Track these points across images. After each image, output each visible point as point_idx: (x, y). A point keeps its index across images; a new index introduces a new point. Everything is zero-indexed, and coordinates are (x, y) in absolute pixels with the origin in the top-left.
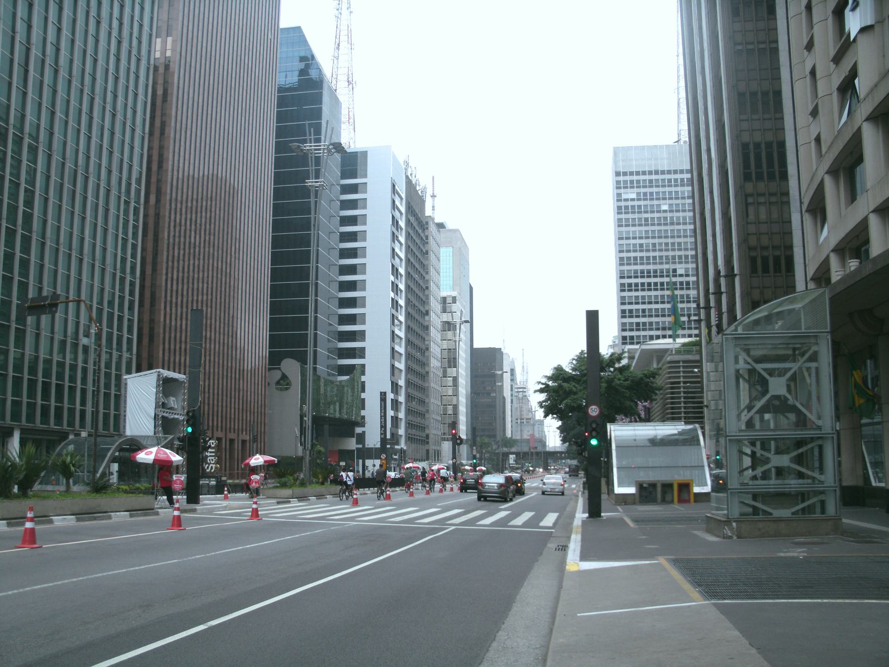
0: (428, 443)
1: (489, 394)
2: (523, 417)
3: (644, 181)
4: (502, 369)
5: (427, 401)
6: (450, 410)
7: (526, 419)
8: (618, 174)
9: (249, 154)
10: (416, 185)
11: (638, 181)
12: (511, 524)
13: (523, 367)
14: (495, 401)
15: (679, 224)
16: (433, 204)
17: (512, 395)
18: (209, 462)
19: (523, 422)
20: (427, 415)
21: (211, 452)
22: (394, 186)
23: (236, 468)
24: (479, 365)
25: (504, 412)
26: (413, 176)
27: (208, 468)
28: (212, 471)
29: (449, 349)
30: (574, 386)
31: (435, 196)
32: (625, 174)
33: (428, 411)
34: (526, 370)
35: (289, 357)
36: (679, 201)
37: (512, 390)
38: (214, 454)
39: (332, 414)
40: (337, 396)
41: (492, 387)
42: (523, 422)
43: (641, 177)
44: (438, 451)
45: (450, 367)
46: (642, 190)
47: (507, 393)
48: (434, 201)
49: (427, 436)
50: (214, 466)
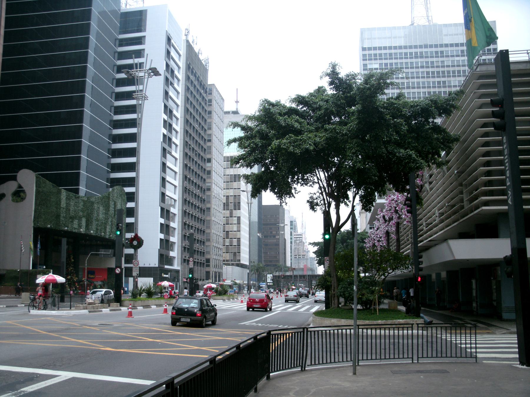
0: (208, 266)
1: (274, 236)
2: (299, 254)
3: (385, 54)
4: (284, 223)
5: (207, 231)
6: (235, 242)
7: (302, 255)
8: (364, 49)
10: (199, 54)
11: (380, 55)
12: (310, 311)
13: (302, 224)
14: (279, 242)
15: (413, 88)
16: (237, 107)
17: (291, 239)
19: (300, 257)
20: (207, 244)
22: (169, 40)
24: (268, 217)
25: (285, 249)
26: (195, 44)
29: (234, 196)
30: (297, 121)
31: (238, 102)
32: (370, 49)
33: (209, 240)
34: (304, 226)
35: (25, 168)
36: (414, 70)
37: (291, 235)
39: (75, 229)
40: (83, 211)
41: (277, 232)
42: (300, 257)
43: (383, 52)
44: (219, 273)
45: (235, 209)
46: (384, 61)
47: (287, 237)
48: (237, 105)
49: (208, 261)
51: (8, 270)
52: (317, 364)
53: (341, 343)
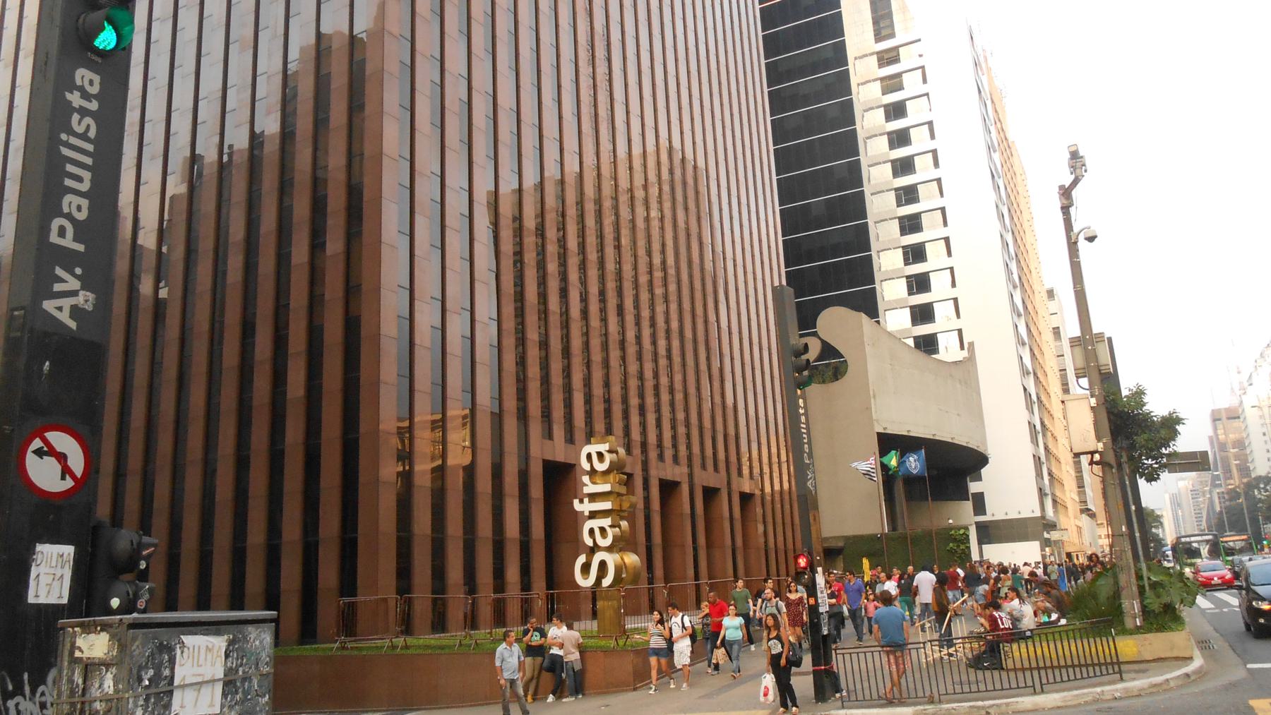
9: (758, 373)
18: (589, 542)
21: (594, 497)
23: (691, 572)
27: (586, 568)
28: (607, 582)
38: (607, 505)
50: (611, 560)
51: (847, 538)
52: (1052, 683)
53: (1076, 656)
